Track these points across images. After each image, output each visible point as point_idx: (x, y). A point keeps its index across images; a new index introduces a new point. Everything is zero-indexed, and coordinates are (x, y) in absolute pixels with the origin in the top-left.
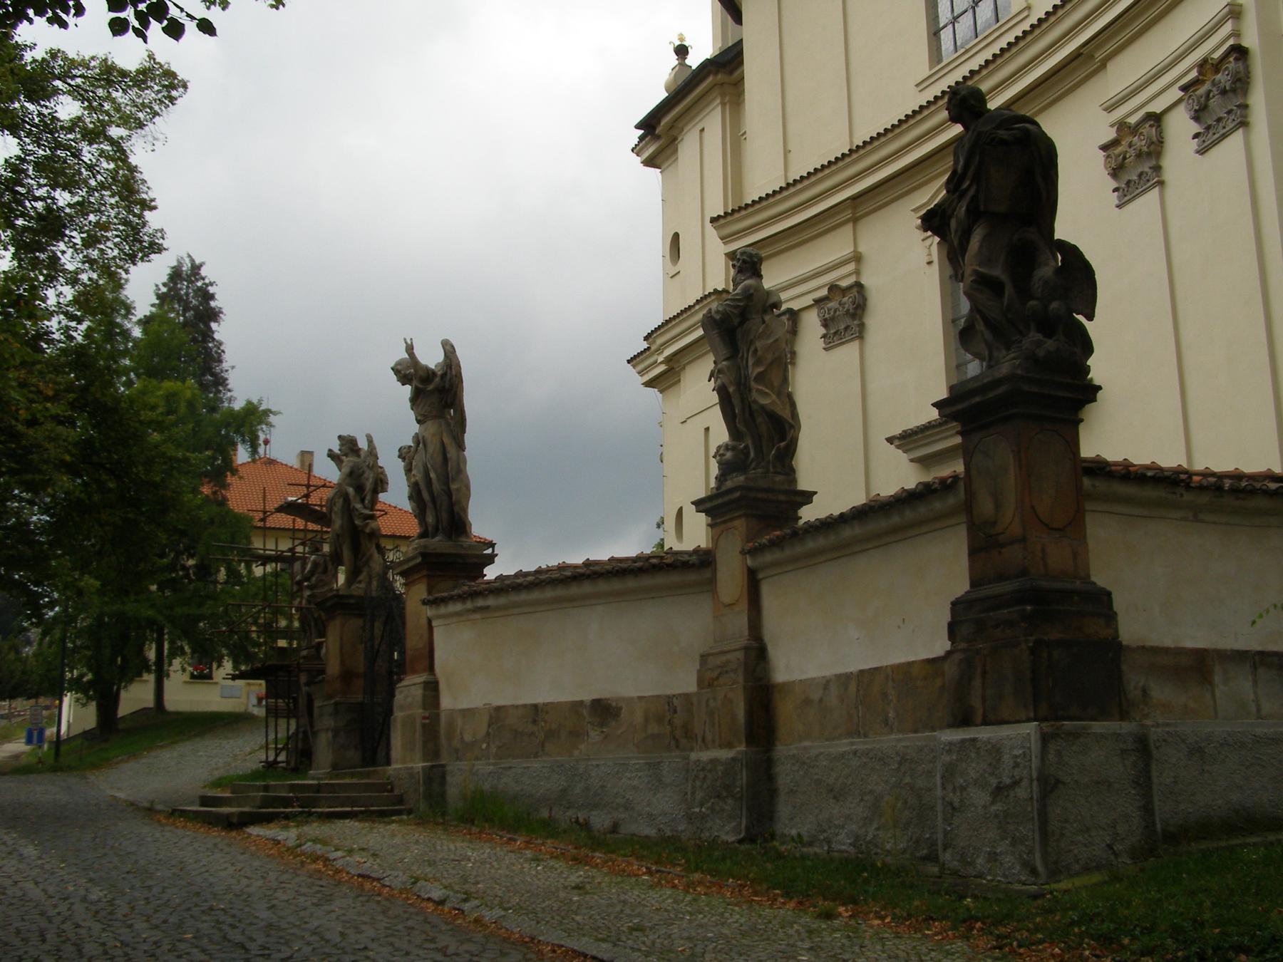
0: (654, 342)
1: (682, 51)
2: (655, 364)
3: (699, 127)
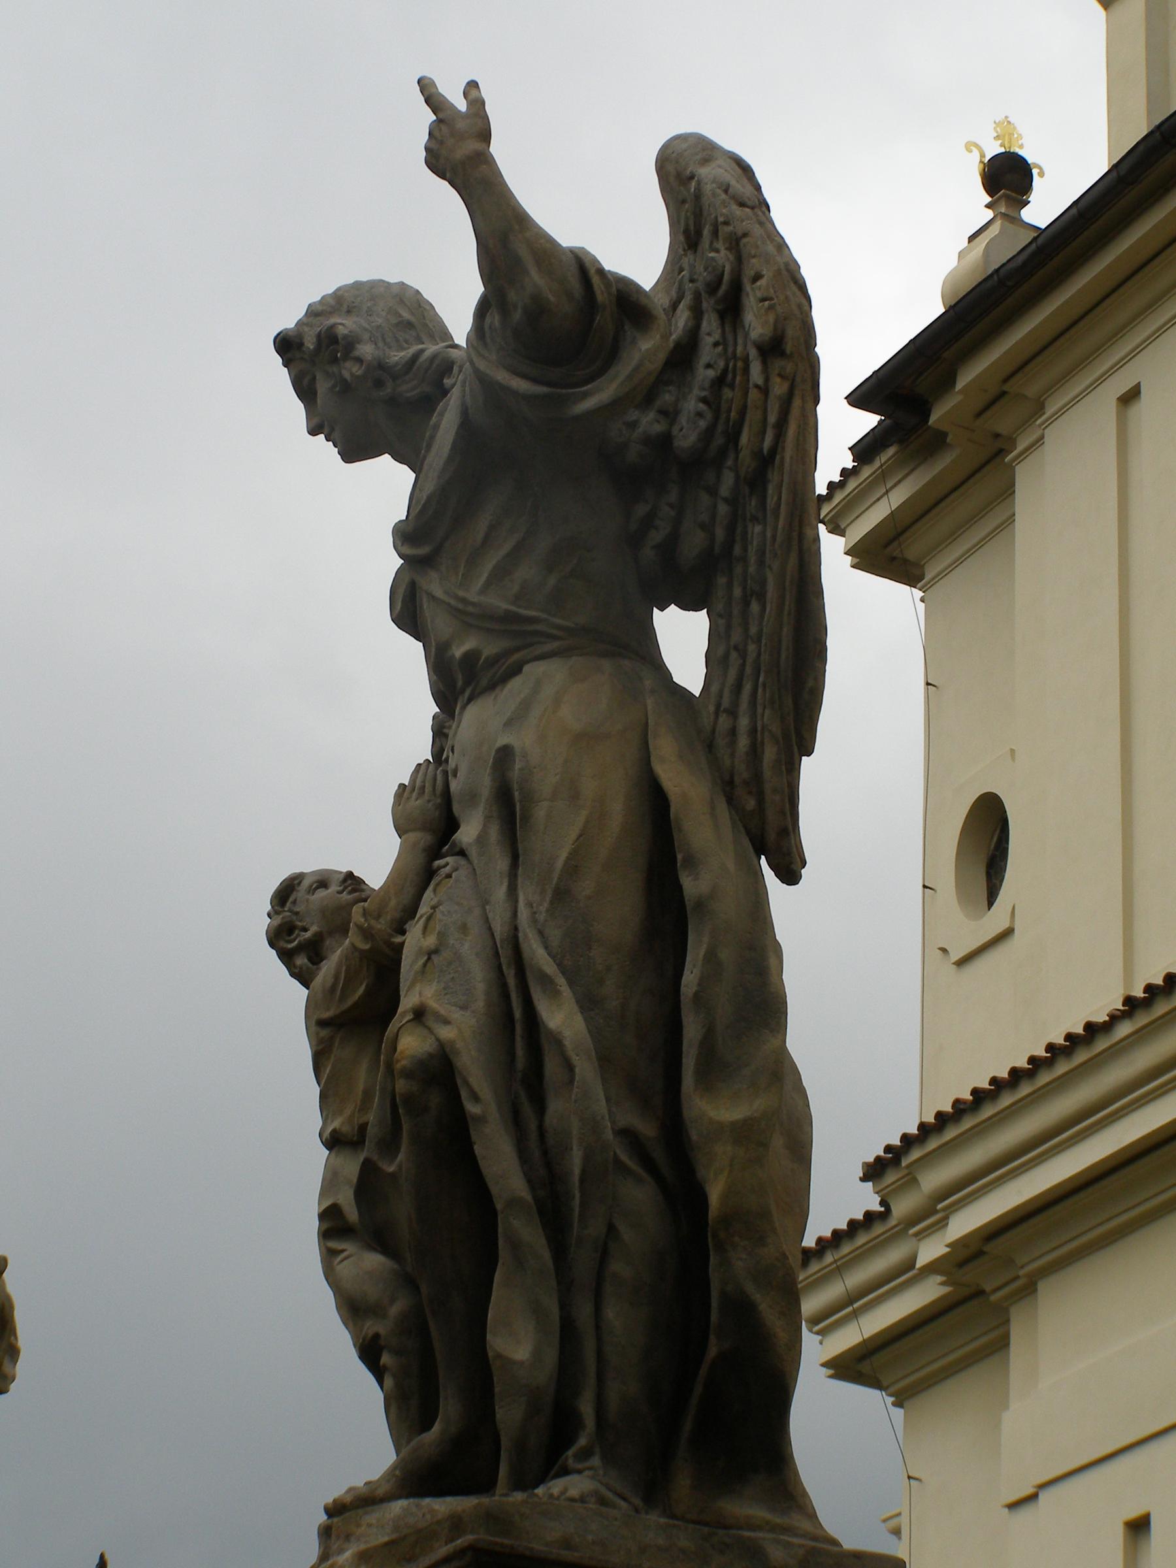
0: (911, 1181)
1: (1008, 177)
2: (905, 1274)
3: (1120, 384)
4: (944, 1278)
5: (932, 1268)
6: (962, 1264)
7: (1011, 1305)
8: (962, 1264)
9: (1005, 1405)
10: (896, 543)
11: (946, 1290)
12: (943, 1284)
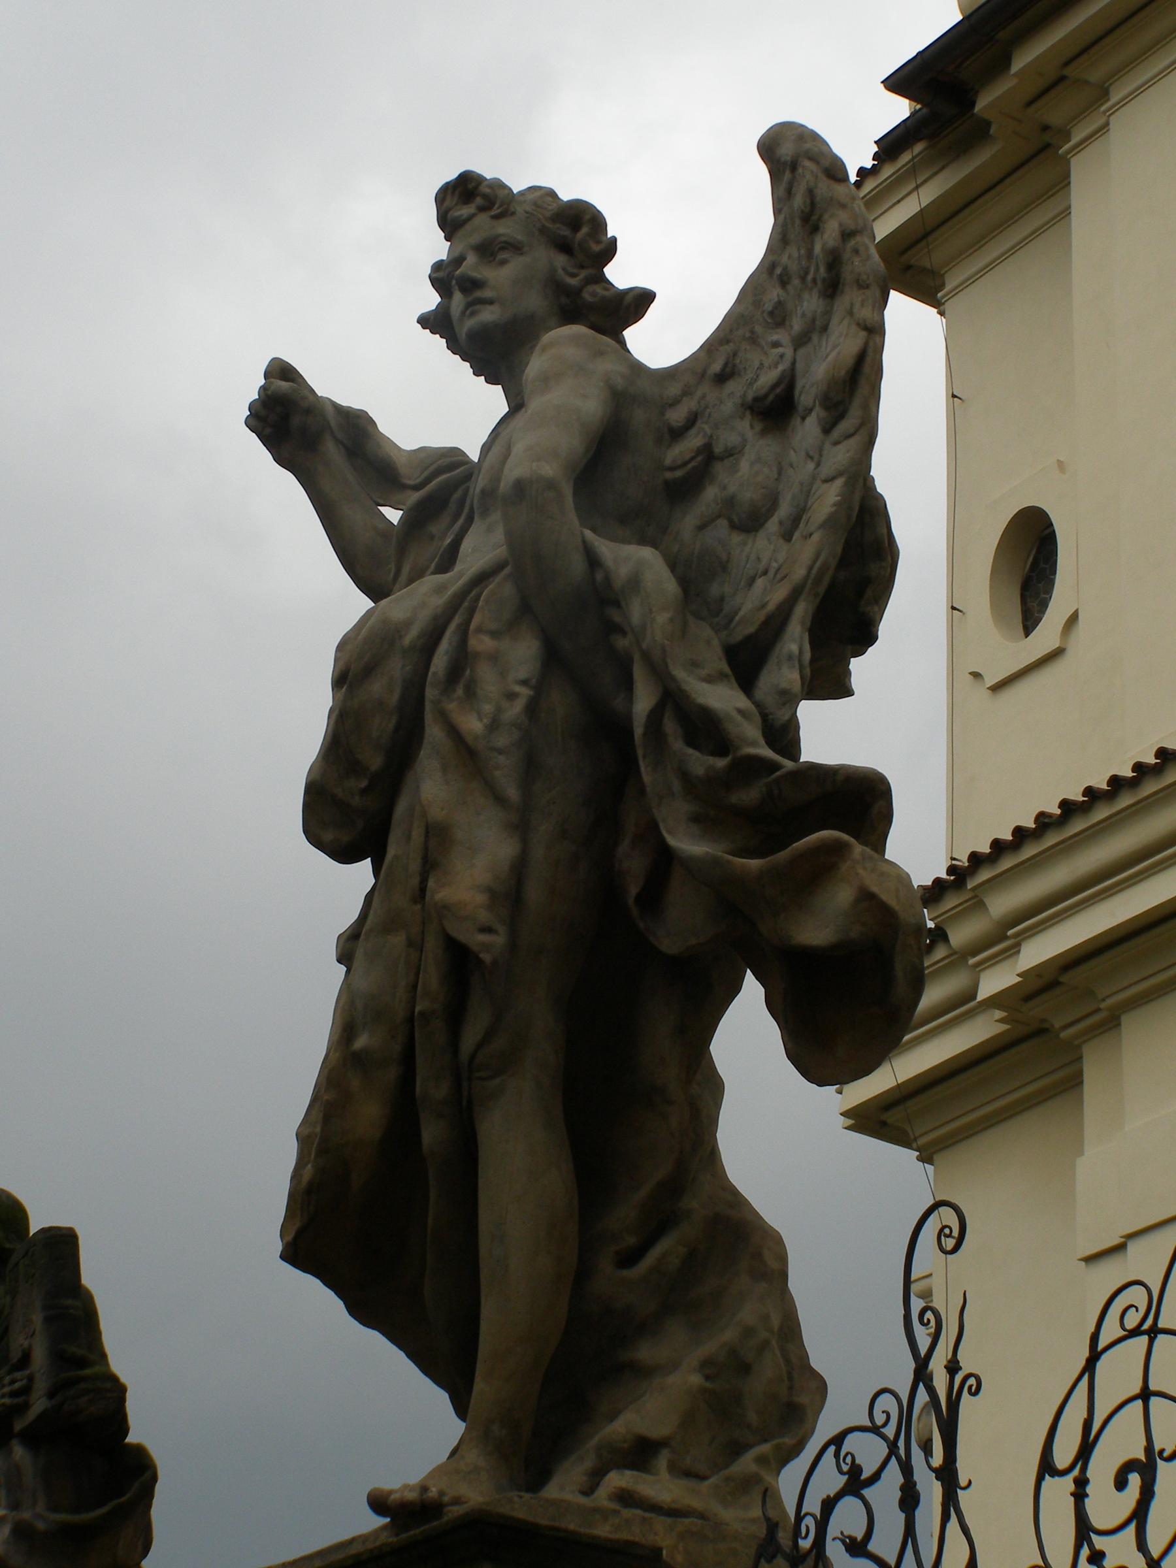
0: (977, 904)
4: (1004, 1014)
5: (994, 1002)
6: (1028, 998)
7: (1084, 1042)
8: (1028, 998)
9: (1081, 1152)
10: (924, 243)
11: (1004, 1027)
12: (1001, 1021)
